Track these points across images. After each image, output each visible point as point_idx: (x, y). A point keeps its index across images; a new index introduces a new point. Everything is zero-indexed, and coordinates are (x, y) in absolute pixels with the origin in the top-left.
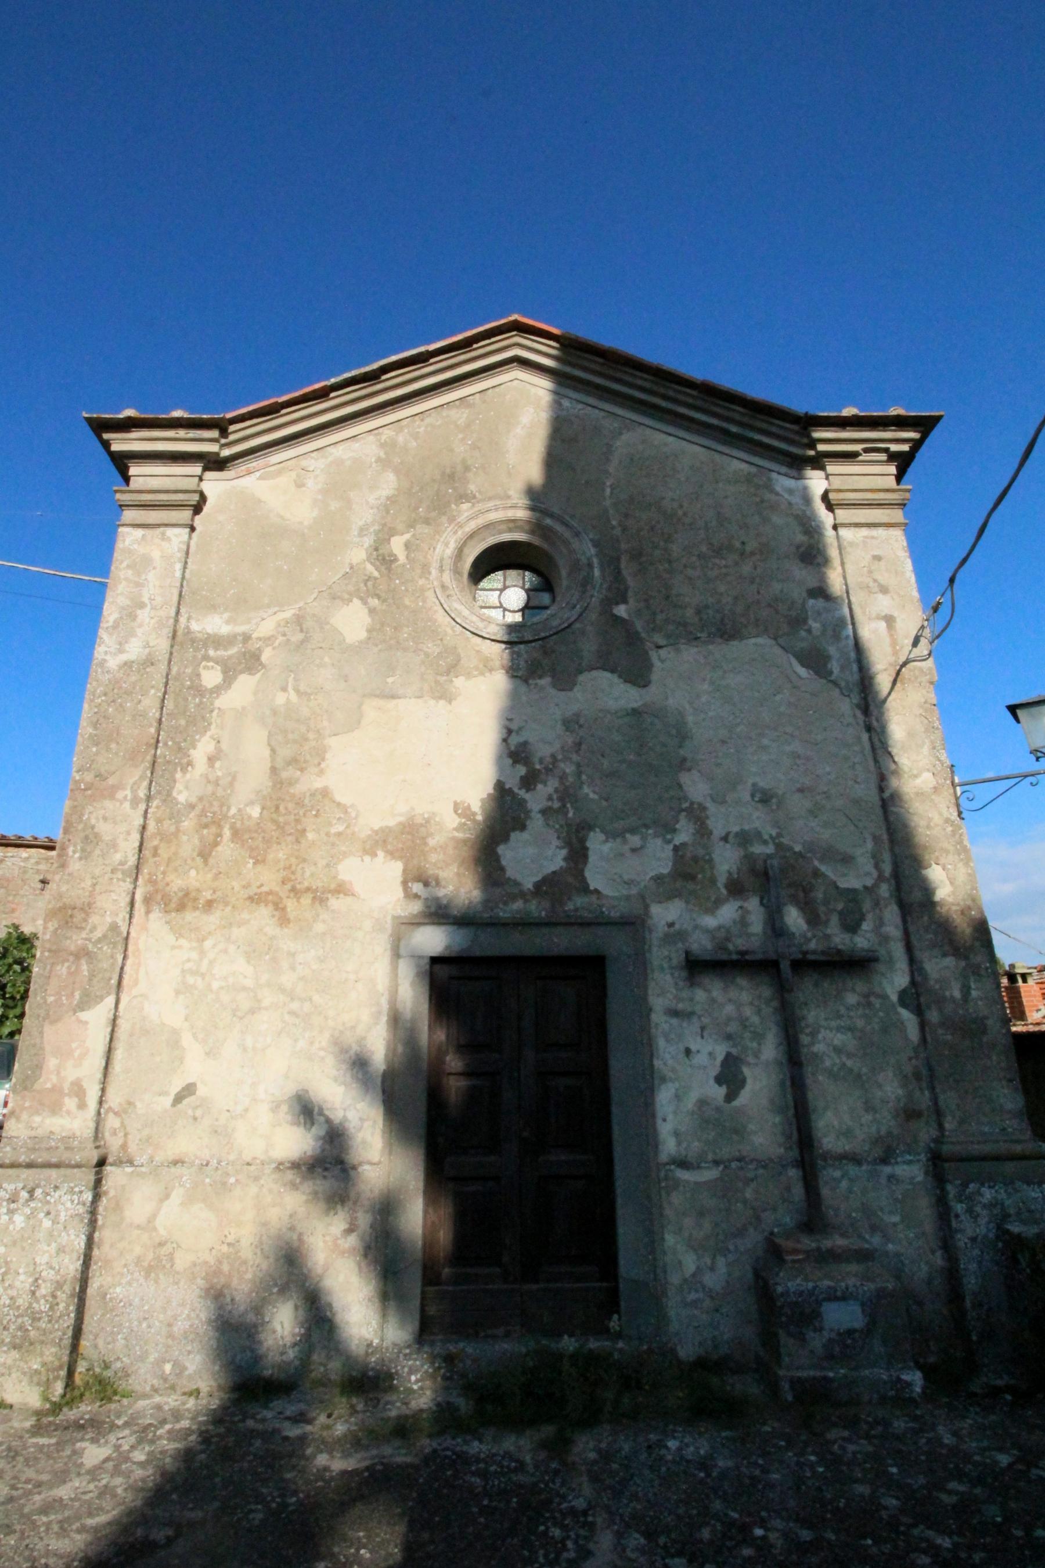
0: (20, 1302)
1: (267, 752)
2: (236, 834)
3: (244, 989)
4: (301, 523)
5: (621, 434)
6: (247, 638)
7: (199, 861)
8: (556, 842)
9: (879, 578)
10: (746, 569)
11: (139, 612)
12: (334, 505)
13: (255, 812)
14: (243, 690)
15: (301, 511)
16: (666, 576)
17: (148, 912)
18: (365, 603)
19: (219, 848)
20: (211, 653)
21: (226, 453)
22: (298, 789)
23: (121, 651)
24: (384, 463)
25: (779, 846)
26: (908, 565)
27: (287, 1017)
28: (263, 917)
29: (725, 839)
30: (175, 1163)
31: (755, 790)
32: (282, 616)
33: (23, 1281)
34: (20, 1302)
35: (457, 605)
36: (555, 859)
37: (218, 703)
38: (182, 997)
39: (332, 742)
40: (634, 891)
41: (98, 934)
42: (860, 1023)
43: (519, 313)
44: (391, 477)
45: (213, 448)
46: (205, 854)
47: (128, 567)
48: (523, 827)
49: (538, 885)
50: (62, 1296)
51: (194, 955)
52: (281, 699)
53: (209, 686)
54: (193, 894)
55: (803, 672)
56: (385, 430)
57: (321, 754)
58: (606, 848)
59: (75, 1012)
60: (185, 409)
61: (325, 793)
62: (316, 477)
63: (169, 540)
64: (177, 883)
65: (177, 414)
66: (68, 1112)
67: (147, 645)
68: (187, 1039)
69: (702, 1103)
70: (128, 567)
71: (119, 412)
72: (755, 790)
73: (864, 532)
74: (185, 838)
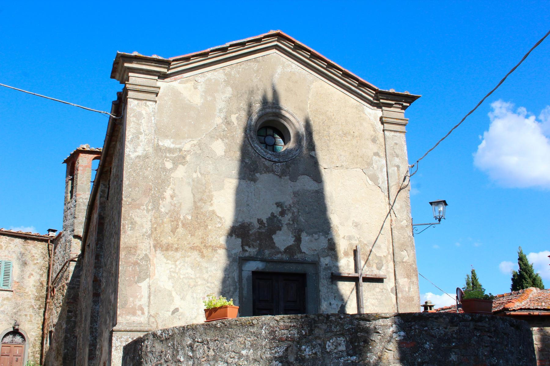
1: (192, 196)
2: (183, 225)
3: (191, 278)
4: (197, 104)
5: (313, 82)
6: (180, 150)
7: (171, 233)
8: (291, 235)
9: (396, 151)
10: (354, 142)
11: (140, 136)
12: (209, 98)
13: (189, 217)
14: (180, 172)
15: (197, 100)
16: (328, 142)
17: (156, 251)
18: (223, 140)
19: (178, 230)
20: (168, 155)
21: (170, 72)
22: (203, 210)
23: (135, 151)
24: (227, 83)
25: (360, 241)
26: (405, 148)
27: (206, 288)
29: (344, 238)
31: (354, 222)
32: (193, 142)
35: (256, 145)
36: (291, 241)
37: (172, 175)
38: (170, 280)
39: (214, 193)
40: (316, 253)
41: (141, 257)
43: (281, 29)
44: (229, 89)
45: (165, 70)
46: (174, 231)
47: (133, 116)
48: (280, 230)
49: (286, 249)
51: (173, 266)
52: (195, 176)
53: (169, 168)
54: (171, 245)
55: (370, 182)
56: (226, 68)
57: (211, 197)
58: (307, 238)
59: (136, 283)
61: (213, 212)
62: (201, 85)
63: (148, 106)
64: (164, 241)
65: (155, 56)
66: (139, 315)
67: (145, 150)
68: (174, 294)
70: (133, 116)
71: (132, 53)
72: (354, 222)
73: (393, 133)
74: (166, 225)
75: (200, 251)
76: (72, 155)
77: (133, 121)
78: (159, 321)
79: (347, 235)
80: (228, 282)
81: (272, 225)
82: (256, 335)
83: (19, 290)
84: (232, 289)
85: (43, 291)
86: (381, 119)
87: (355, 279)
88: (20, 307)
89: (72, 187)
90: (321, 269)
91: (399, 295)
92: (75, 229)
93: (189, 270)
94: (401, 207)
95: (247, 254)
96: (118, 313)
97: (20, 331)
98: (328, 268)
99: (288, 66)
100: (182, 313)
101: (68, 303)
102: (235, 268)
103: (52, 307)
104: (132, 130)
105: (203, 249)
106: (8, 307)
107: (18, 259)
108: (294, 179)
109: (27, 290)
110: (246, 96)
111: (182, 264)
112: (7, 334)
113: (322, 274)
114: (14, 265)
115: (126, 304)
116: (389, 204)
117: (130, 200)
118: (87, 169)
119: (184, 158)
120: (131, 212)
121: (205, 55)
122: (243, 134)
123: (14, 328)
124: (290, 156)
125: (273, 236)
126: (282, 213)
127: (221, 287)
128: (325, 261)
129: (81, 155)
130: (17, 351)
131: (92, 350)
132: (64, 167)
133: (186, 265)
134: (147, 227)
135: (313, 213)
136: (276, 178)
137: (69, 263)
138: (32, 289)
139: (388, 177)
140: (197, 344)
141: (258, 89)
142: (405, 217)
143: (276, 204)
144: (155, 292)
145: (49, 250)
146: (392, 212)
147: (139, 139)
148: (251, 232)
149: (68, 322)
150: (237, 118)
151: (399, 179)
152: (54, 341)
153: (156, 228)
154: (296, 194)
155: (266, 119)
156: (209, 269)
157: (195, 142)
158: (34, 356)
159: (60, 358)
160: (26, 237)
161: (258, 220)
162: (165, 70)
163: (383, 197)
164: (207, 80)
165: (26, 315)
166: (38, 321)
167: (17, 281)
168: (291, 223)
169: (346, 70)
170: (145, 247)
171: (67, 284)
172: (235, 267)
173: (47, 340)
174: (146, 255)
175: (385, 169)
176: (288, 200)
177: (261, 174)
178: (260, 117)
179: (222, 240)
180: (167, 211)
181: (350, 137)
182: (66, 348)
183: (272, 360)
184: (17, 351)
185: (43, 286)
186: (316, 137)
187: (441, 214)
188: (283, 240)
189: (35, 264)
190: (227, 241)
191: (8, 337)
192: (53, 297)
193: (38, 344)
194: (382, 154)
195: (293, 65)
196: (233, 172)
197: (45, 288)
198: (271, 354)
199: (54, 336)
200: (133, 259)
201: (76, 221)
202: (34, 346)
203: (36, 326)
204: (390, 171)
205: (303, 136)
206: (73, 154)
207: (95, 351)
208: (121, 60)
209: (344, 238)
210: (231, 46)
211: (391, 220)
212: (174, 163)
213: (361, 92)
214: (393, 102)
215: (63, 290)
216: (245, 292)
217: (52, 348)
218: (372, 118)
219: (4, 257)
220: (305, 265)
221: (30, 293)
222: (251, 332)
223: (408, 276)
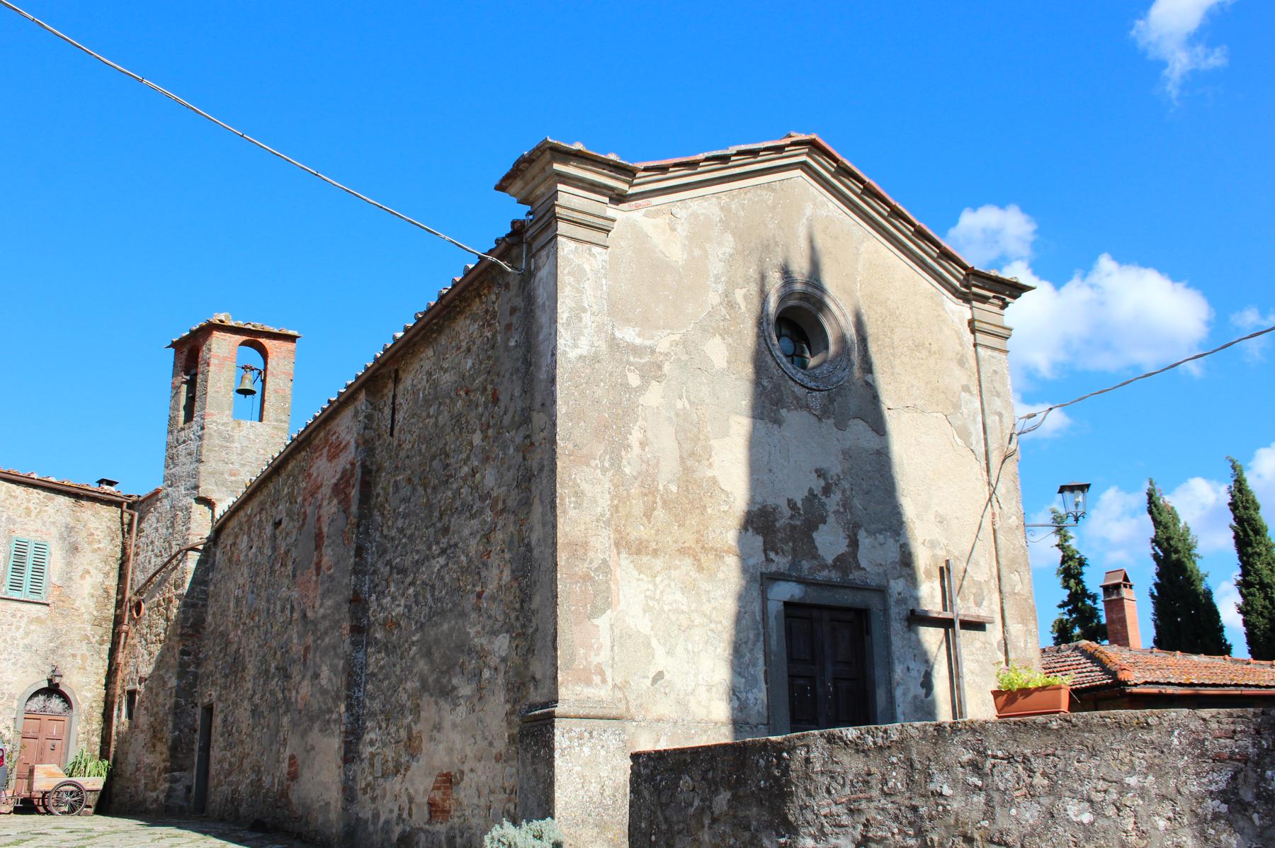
1: (675, 445)
3: (683, 612)
7: (645, 519)
8: (842, 534)
12: (697, 252)
13: (674, 488)
14: (653, 396)
15: (676, 253)
17: (619, 553)
19: (656, 513)
20: (631, 359)
21: (631, 191)
23: (576, 346)
25: (948, 551)
30: (658, 720)
31: (937, 515)
33: (594, 787)
37: (641, 400)
39: (713, 442)
40: (881, 570)
41: (595, 565)
44: (729, 238)
45: (624, 186)
46: (648, 514)
48: (825, 522)
50: (619, 796)
51: (651, 587)
52: (679, 405)
57: (708, 450)
60: (618, 154)
61: (714, 481)
64: (634, 535)
68: (654, 643)
69: (915, 697)
71: (571, 143)
72: (937, 515)
75: (694, 557)
76: (194, 334)
78: (631, 697)
79: (928, 538)
80: (744, 622)
81: (810, 516)
82: (1161, 749)
83: (61, 604)
84: (751, 636)
86: (971, 323)
87: (947, 624)
88: (64, 638)
89: (191, 400)
90: (892, 601)
91: (1012, 655)
93: (679, 596)
94: (1008, 491)
95: (773, 568)
96: (560, 679)
97: (61, 688)
98: (902, 601)
101: (182, 635)
103: (136, 641)
104: (568, 301)
105: (699, 552)
106: (39, 637)
107: (62, 538)
108: (841, 425)
109: (77, 604)
111: (666, 582)
112: (36, 694)
113: (894, 611)
115: (572, 660)
116: (989, 483)
117: (570, 446)
119: (660, 367)
120: (574, 471)
123: (50, 681)
124: (835, 380)
125: (814, 535)
126: (827, 490)
127: (733, 632)
128: (897, 586)
129: (216, 334)
130: (54, 728)
132: (169, 357)
133: (673, 584)
134: (604, 503)
135: (870, 491)
136: (814, 420)
137: (186, 554)
138: (86, 601)
139: (985, 433)
141: (776, 244)
142: (1014, 510)
143: (816, 471)
146: (994, 499)
147: (580, 321)
148: (778, 525)
149: (181, 675)
150: (745, 297)
151: (1002, 438)
153: (617, 507)
154: (847, 454)
155: (805, 305)
156: (712, 595)
157: (677, 337)
158: (89, 741)
159: (163, 748)
160: (77, 495)
161: (789, 501)
162: (624, 186)
163: (979, 468)
165: (74, 656)
167: (58, 583)
169: (923, 226)
170: (601, 542)
171: (179, 597)
172: (755, 593)
173: (120, 709)
174: (604, 561)
175: (980, 419)
176: (835, 467)
179: (731, 537)
181: (924, 353)
182: (176, 727)
183: (1203, 798)
184: (54, 728)
185: (108, 597)
186: (873, 348)
187: (1081, 509)
188: (829, 541)
189: (95, 551)
190: (740, 541)
191: (36, 699)
194: (975, 390)
195: (830, 204)
197: (114, 601)
198: (1200, 784)
199: (141, 702)
200: (582, 568)
201: (202, 468)
202: (88, 721)
203: (93, 679)
204: (988, 422)
206: (197, 331)
208: (548, 155)
210: (739, 153)
211: (994, 514)
213: (941, 270)
214: (991, 294)
215: (167, 609)
217: (136, 727)
218: (956, 320)
219: (32, 534)
220: (867, 594)
221: (83, 610)
222: (1145, 741)
223: (1023, 621)
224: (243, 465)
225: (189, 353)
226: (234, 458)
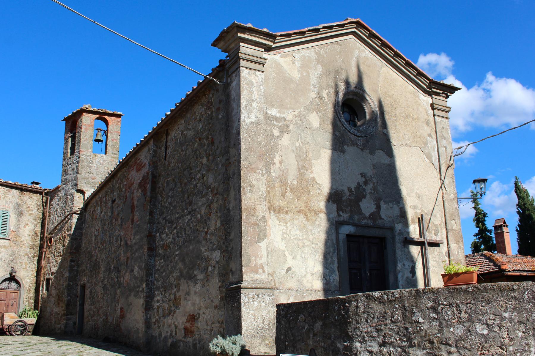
0: (260, 326)
1: (296, 163)
2: (291, 189)
3: (300, 239)
8: (373, 203)
10: (414, 123)
12: (305, 74)
13: (295, 183)
14: (285, 140)
15: (295, 74)
17: (270, 213)
19: (287, 194)
20: (275, 123)
21: (274, 46)
23: (249, 118)
24: (318, 60)
28: (301, 218)
29: (411, 207)
31: (417, 194)
33: (260, 320)
34: (260, 326)
36: (373, 209)
37: (280, 142)
39: (313, 161)
40: (391, 220)
41: (259, 218)
42: (438, 259)
44: (320, 67)
45: (271, 44)
46: (283, 195)
48: (365, 198)
51: (285, 228)
52: (297, 144)
55: (427, 160)
57: (311, 165)
58: (385, 206)
60: (268, 29)
61: (314, 179)
65: (265, 30)
67: (257, 117)
68: (287, 254)
69: (407, 278)
72: (417, 194)
74: (277, 189)
77: (246, 89)
78: (276, 279)
81: (358, 194)
83: (15, 239)
84: (332, 250)
85: (37, 240)
86: (432, 105)
87: (421, 244)
89: (73, 145)
90: (396, 234)
91: (452, 258)
92: (79, 183)
93: (298, 232)
94: (450, 183)
95: (341, 219)
96: (243, 271)
98: (401, 233)
99: (363, 51)
100: (294, 272)
101: (70, 253)
102: (333, 231)
103: (50, 256)
104: (245, 97)
105: (307, 212)
106: (5, 254)
107: (15, 209)
108: (372, 153)
110: (333, 75)
111: (292, 226)
113: (397, 238)
114: (11, 214)
115: (249, 262)
117: (247, 164)
118: (90, 127)
119: (288, 127)
120: (249, 175)
121: (303, 33)
122: (332, 109)
123: (11, 274)
124: (369, 132)
125: (360, 203)
126: (366, 183)
128: (399, 227)
129: (84, 114)
130: (13, 296)
131: (148, 301)
133: (295, 227)
134: (263, 190)
135: (386, 183)
136: (359, 151)
137: (72, 216)
140: (442, 306)
142: (452, 191)
143: (361, 174)
144: (271, 251)
145: (43, 202)
146: (443, 186)
149: (71, 270)
150: (327, 94)
151: (447, 158)
152: (53, 288)
153: (269, 191)
154: (375, 166)
157: (296, 113)
160: (22, 189)
162: (271, 44)
163: (436, 172)
164: (302, 56)
165: (21, 263)
166: (32, 268)
167: (14, 230)
168: (373, 192)
170: (262, 208)
171: (69, 235)
173: (43, 287)
174: (263, 217)
175: (436, 149)
176: (370, 172)
177: (348, 147)
178: (345, 95)
179: (322, 205)
180: (277, 176)
181: (410, 119)
182: (68, 295)
184: (13, 296)
185: (37, 236)
186: (387, 117)
188: (367, 206)
189: (30, 215)
190: (327, 207)
192: (49, 247)
193: (32, 290)
194: (434, 136)
196: (327, 143)
199: (52, 284)
200: (253, 220)
201: (79, 176)
202: (28, 292)
204: (440, 151)
205: (377, 114)
207: (151, 302)
208: (235, 30)
209: (411, 207)
212: (280, 131)
213: (418, 81)
214: (441, 92)
215: (64, 241)
216: (342, 253)
217: (50, 295)
218: (425, 104)
221: (25, 242)
223: (457, 242)
224: (98, 174)
225: (72, 124)
226: (93, 171)
